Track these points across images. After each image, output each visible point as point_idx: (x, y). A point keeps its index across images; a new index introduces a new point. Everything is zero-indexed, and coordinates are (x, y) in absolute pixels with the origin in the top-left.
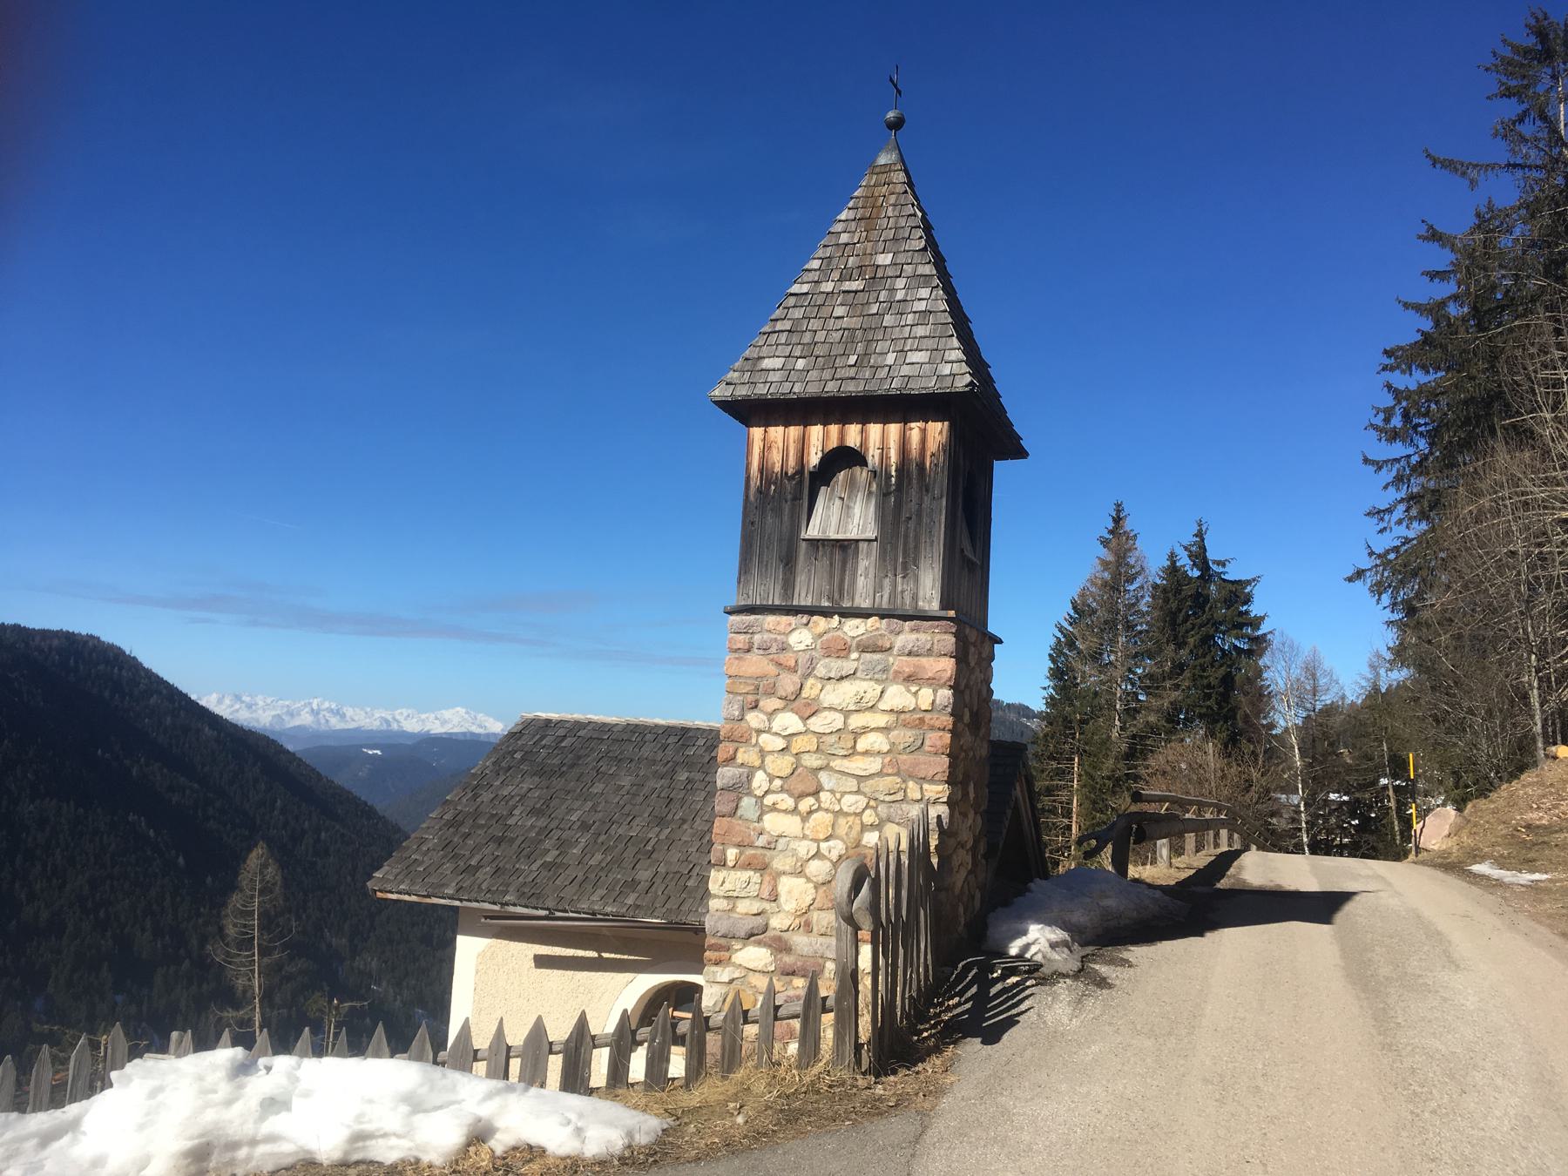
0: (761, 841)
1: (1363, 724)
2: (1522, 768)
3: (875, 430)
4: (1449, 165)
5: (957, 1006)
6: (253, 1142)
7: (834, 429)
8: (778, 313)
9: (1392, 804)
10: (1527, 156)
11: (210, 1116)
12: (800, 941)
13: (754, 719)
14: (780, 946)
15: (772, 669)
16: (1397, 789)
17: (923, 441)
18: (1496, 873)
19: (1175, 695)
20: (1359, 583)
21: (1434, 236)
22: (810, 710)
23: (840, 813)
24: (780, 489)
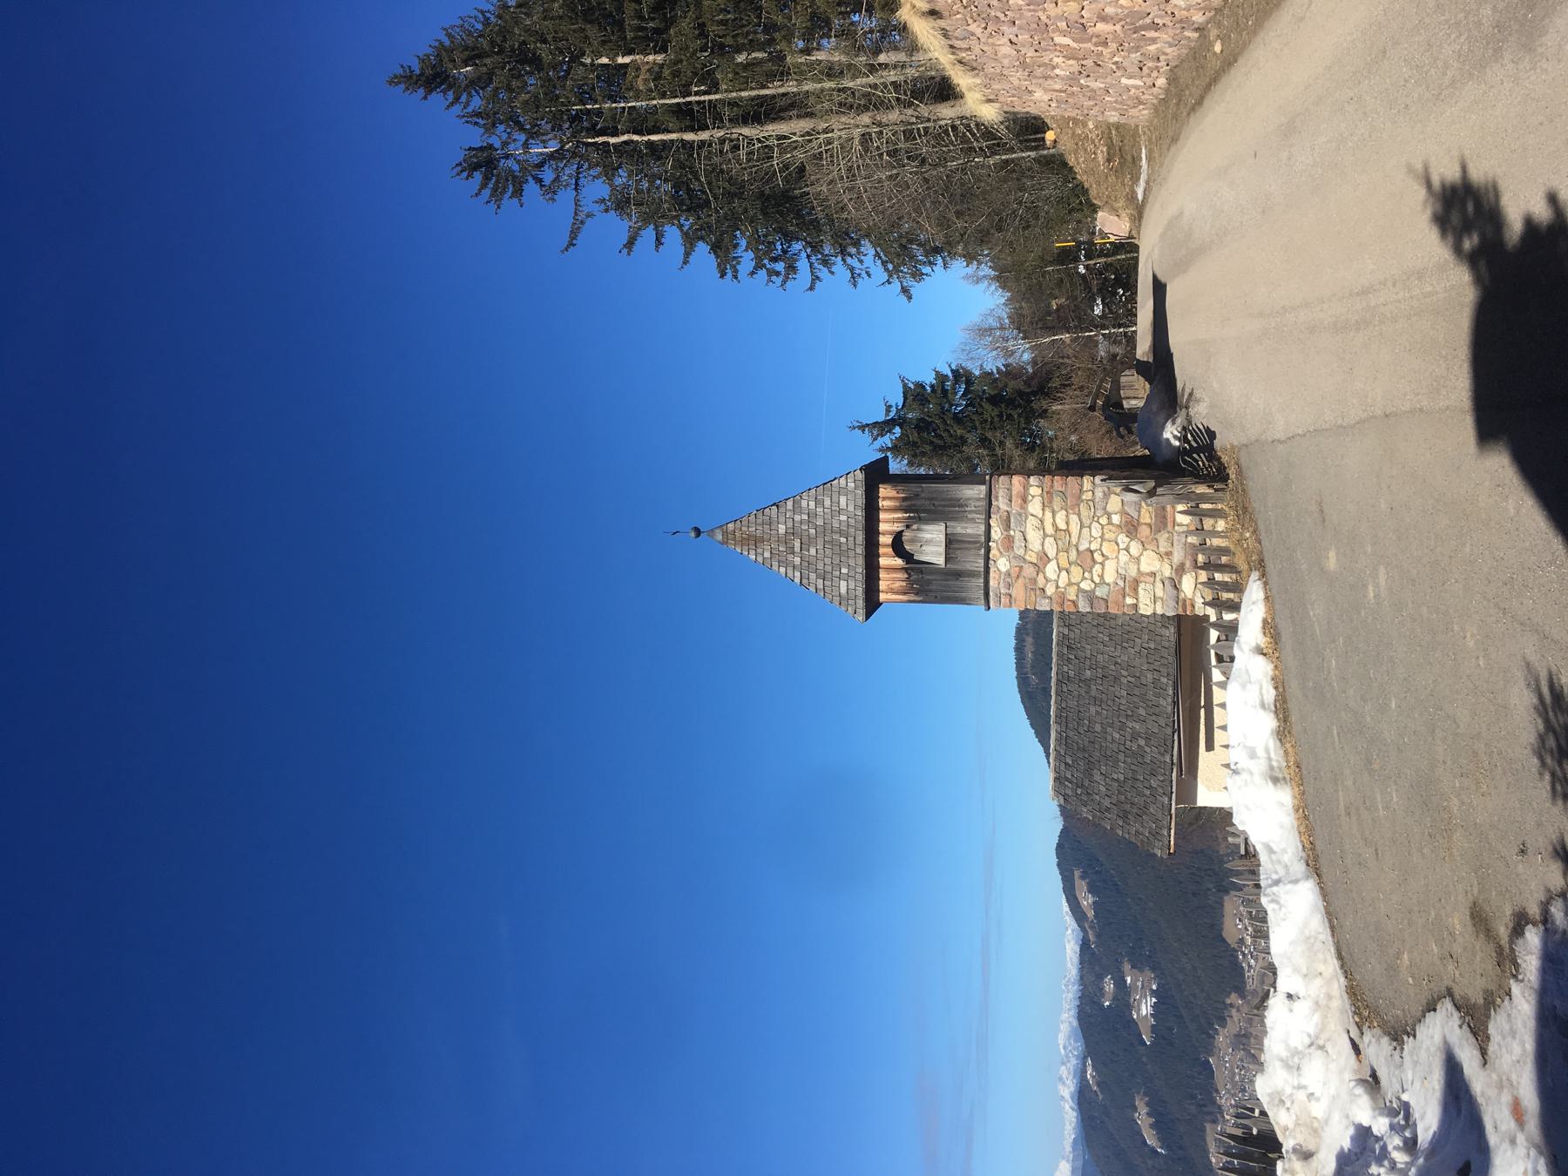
1: (1030, 288)
2: (1065, 164)
3: (883, 527)
4: (574, 234)
5: (1202, 460)
6: (1270, 759)
7: (881, 550)
8: (812, 589)
9: (1102, 260)
10: (570, 176)
11: (1258, 779)
12: (1177, 557)
13: (1050, 590)
14: (1180, 570)
15: (1021, 581)
16: (1088, 257)
17: (890, 498)
18: (1142, 183)
19: (1009, 443)
20: (913, 291)
21: (630, 244)
22: (1044, 558)
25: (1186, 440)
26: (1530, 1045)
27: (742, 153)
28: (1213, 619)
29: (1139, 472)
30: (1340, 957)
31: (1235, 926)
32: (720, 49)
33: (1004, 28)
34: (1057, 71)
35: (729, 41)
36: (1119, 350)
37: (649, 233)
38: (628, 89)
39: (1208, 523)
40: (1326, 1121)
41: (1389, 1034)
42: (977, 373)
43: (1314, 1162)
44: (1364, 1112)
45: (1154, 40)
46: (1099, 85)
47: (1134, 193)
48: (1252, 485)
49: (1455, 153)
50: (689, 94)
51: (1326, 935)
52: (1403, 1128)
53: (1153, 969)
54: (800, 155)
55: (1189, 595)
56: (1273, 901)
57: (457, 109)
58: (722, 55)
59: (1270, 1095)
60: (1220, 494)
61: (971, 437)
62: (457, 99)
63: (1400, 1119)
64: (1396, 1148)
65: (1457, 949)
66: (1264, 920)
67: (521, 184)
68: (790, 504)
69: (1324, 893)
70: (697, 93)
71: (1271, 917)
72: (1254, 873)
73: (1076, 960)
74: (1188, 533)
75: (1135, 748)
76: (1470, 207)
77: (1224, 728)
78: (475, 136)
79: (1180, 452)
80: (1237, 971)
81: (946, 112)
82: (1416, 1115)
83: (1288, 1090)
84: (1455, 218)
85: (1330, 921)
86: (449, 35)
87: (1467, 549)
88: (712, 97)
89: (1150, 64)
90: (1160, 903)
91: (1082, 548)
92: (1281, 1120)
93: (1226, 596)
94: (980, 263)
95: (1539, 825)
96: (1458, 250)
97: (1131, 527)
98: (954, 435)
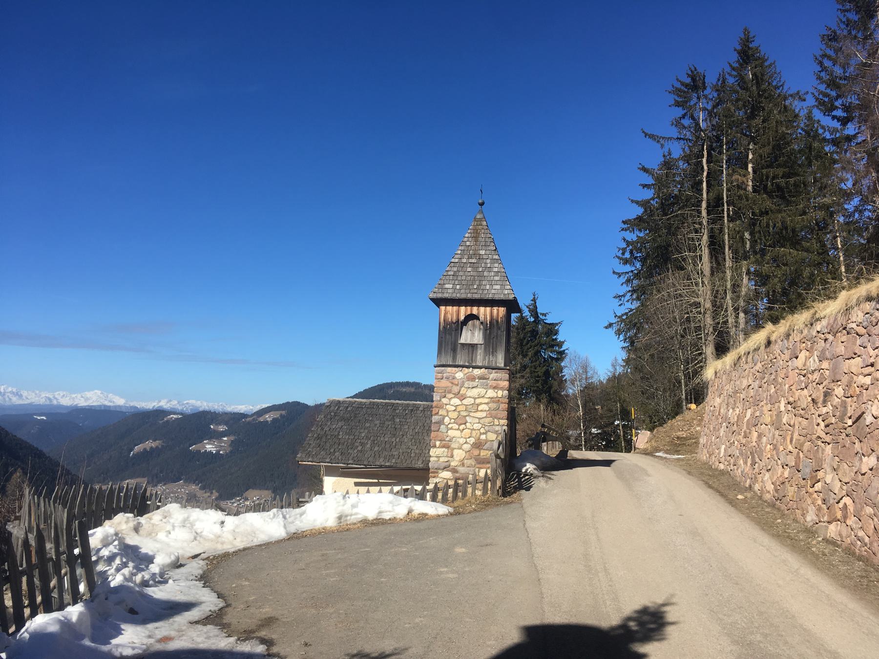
0: (448, 439)
1: (608, 394)
2: (677, 415)
3: (482, 309)
4: (652, 137)
5: (514, 483)
6: (351, 515)
7: (469, 308)
8: (448, 269)
9: (622, 434)
11: (340, 508)
12: (462, 470)
13: (444, 401)
14: (454, 471)
15: (450, 385)
16: (624, 426)
18: (665, 455)
19: (523, 381)
20: (610, 329)
21: (645, 170)
23: (473, 429)
24: (451, 327)
25: (526, 475)
26: (203, 646)
27: (693, 235)
28: (428, 487)
29: (508, 450)
30: (245, 549)
31: (255, 496)
32: (753, 224)
33: (757, 382)
34: (731, 410)
35: (757, 229)
36: (572, 442)
37: (650, 181)
38: (733, 170)
39: (480, 486)
40: (155, 540)
41: (204, 574)
42: (562, 364)
43: (133, 534)
44: (161, 560)
45: (745, 463)
46: (722, 433)
47: (660, 451)
48: (501, 510)
49: (682, 619)
50: (728, 205)
51: (256, 542)
52: (154, 581)
53: (231, 452)
54: (690, 268)
55: (440, 475)
56: (274, 515)
57: (728, 69)
58: (750, 225)
59: (169, 511)
60: (496, 492)
61: (527, 360)
62: (733, 69)
63: (158, 579)
64: (143, 577)
65: (252, 610)
66: (264, 510)
67: (683, 106)
68: (496, 257)
69: (279, 542)
70: (728, 209)
71: (265, 514)
72: (289, 505)
73: (236, 411)
74: (474, 474)
75: (356, 444)
76: (652, 626)
77: (368, 492)
78: (711, 79)
79: (519, 472)
80: (230, 496)
81: (709, 350)
82: (161, 587)
83: (172, 521)
84: (646, 618)
85: (264, 544)
86: (770, 65)
87: (467, 620)
88: (726, 218)
89: (732, 461)
90: (269, 456)
91: (467, 418)
92: (155, 517)
93: (440, 495)
94: (624, 366)
95: (321, 653)
96: (629, 619)
97: (478, 445)
98: (529, 348)
